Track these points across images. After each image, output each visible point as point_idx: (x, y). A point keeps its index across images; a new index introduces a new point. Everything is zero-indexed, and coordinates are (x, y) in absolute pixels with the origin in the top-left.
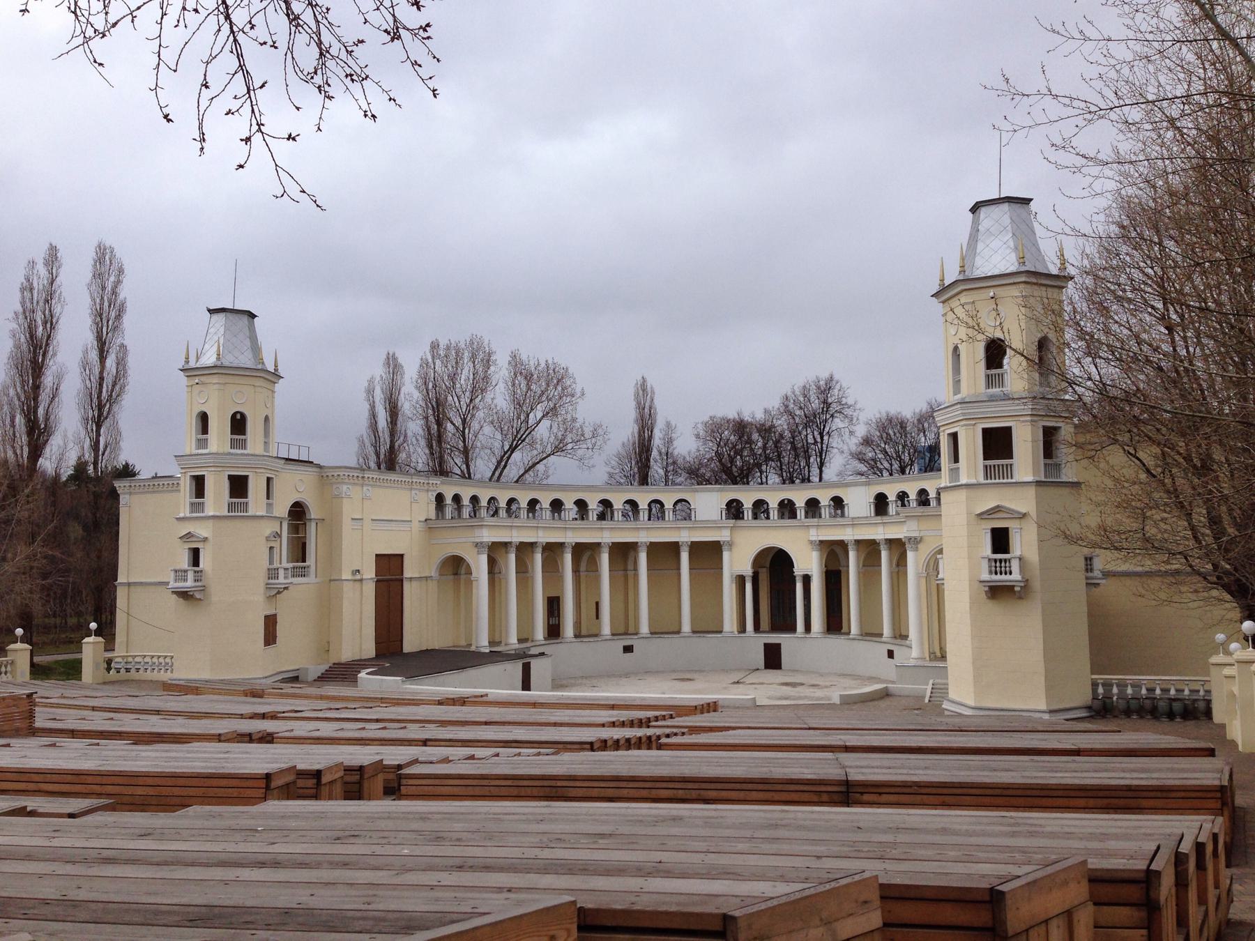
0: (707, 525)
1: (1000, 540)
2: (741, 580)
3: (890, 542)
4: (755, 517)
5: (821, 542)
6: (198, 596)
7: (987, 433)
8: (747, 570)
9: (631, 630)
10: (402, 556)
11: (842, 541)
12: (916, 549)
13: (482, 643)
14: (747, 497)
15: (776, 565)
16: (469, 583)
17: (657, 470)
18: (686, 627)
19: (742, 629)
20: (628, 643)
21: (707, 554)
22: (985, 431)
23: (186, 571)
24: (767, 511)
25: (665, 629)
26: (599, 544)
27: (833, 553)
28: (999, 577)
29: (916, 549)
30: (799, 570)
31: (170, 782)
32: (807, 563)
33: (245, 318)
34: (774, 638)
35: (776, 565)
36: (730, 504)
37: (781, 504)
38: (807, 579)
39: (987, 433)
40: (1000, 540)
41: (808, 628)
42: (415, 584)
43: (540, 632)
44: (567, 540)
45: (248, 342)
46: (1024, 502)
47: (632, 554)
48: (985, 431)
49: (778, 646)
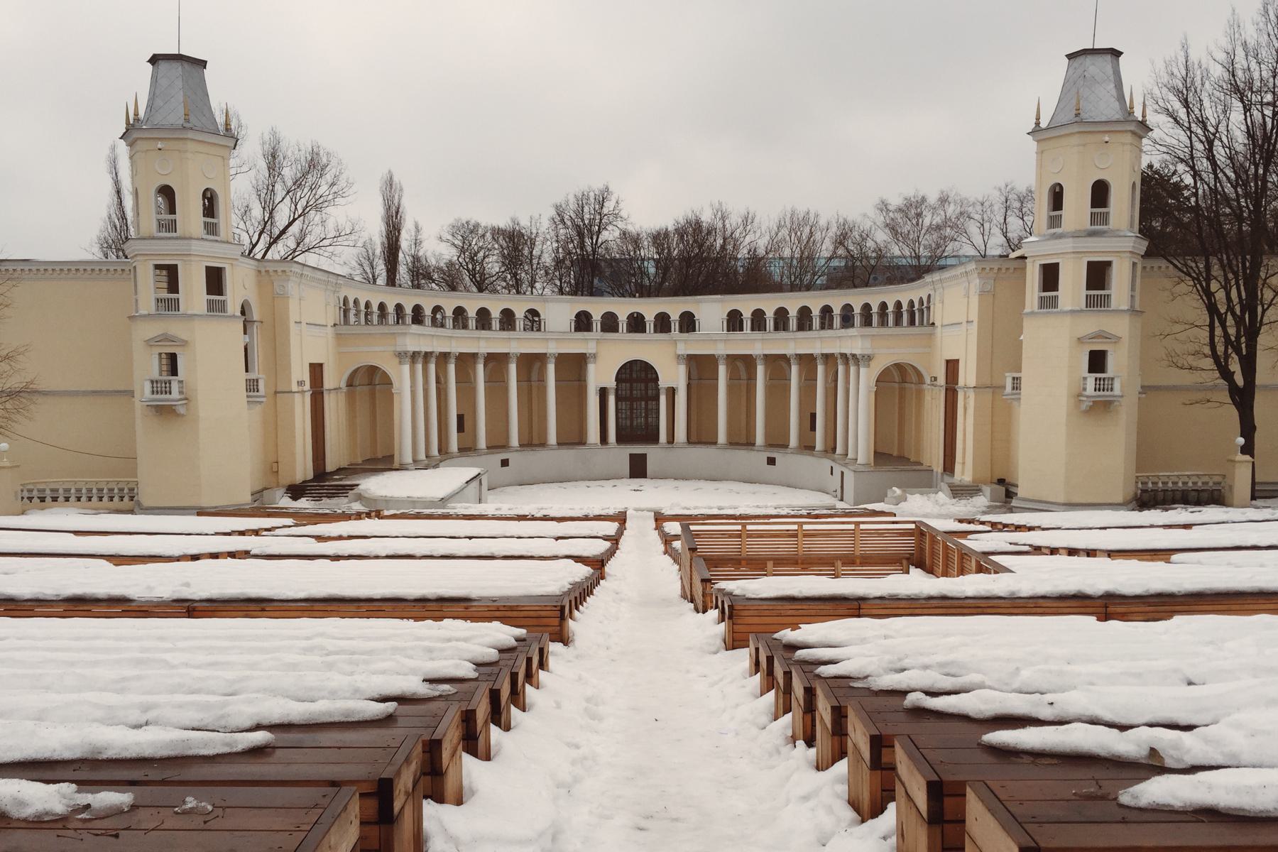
0: (711, 340)
1: (1097, 361)
2: (603, 393)
3: (800, 357)
4: (776, 328)
5: (766, 355)
6: (182, 410)
7: (1091, 265)
8: (611, 383)
9: (535, 441)
10: (321, 365)
11: (785, 355)
12: (869, 366)
13: (895, 454)
14: (597, 307)
15: (637, 377)
16: (389, 397)
17: (403, 272)
18: (552, 438)
19: (604, 439)
20: (504, 456)
21: (574, 366)
22: (1090, 263)
23: (1085, 379)
24: (466, 319)
25: (533, 441)
26: (507, 354)
27: (701, 368)
28: (1101, 393)
29: (869, 366)
30: (664, 383)
31: (917, 611)
32: (672, 375)
33: (1108, 57)
34: (638, 449)
35: (637, 377)
36: (579, 315)
37: (631, 316)
38: (672, 392)
39: (1091, 265)
40: (1097, 361)
41: (671, 440)
42: (333, 395)
43: (435, 452)
44: (512, 351)
45: (1114, 92)
46: (1121, 326)
47: (537, 365)
48: (1090, 263)
49: (644, 456)
